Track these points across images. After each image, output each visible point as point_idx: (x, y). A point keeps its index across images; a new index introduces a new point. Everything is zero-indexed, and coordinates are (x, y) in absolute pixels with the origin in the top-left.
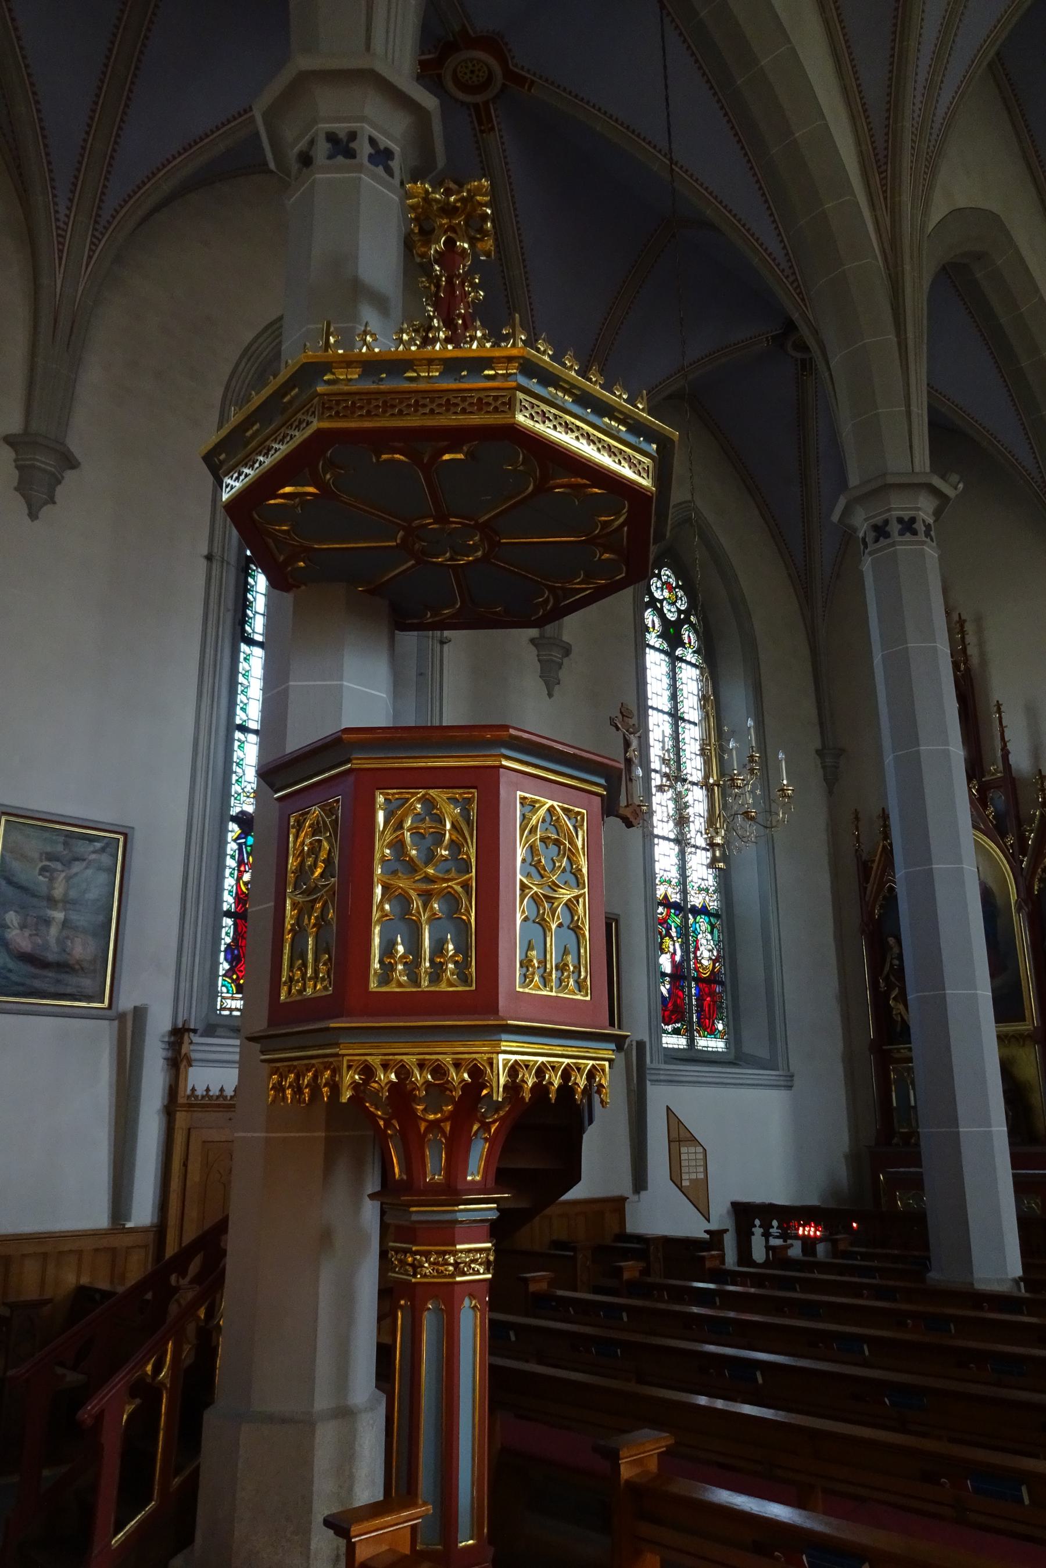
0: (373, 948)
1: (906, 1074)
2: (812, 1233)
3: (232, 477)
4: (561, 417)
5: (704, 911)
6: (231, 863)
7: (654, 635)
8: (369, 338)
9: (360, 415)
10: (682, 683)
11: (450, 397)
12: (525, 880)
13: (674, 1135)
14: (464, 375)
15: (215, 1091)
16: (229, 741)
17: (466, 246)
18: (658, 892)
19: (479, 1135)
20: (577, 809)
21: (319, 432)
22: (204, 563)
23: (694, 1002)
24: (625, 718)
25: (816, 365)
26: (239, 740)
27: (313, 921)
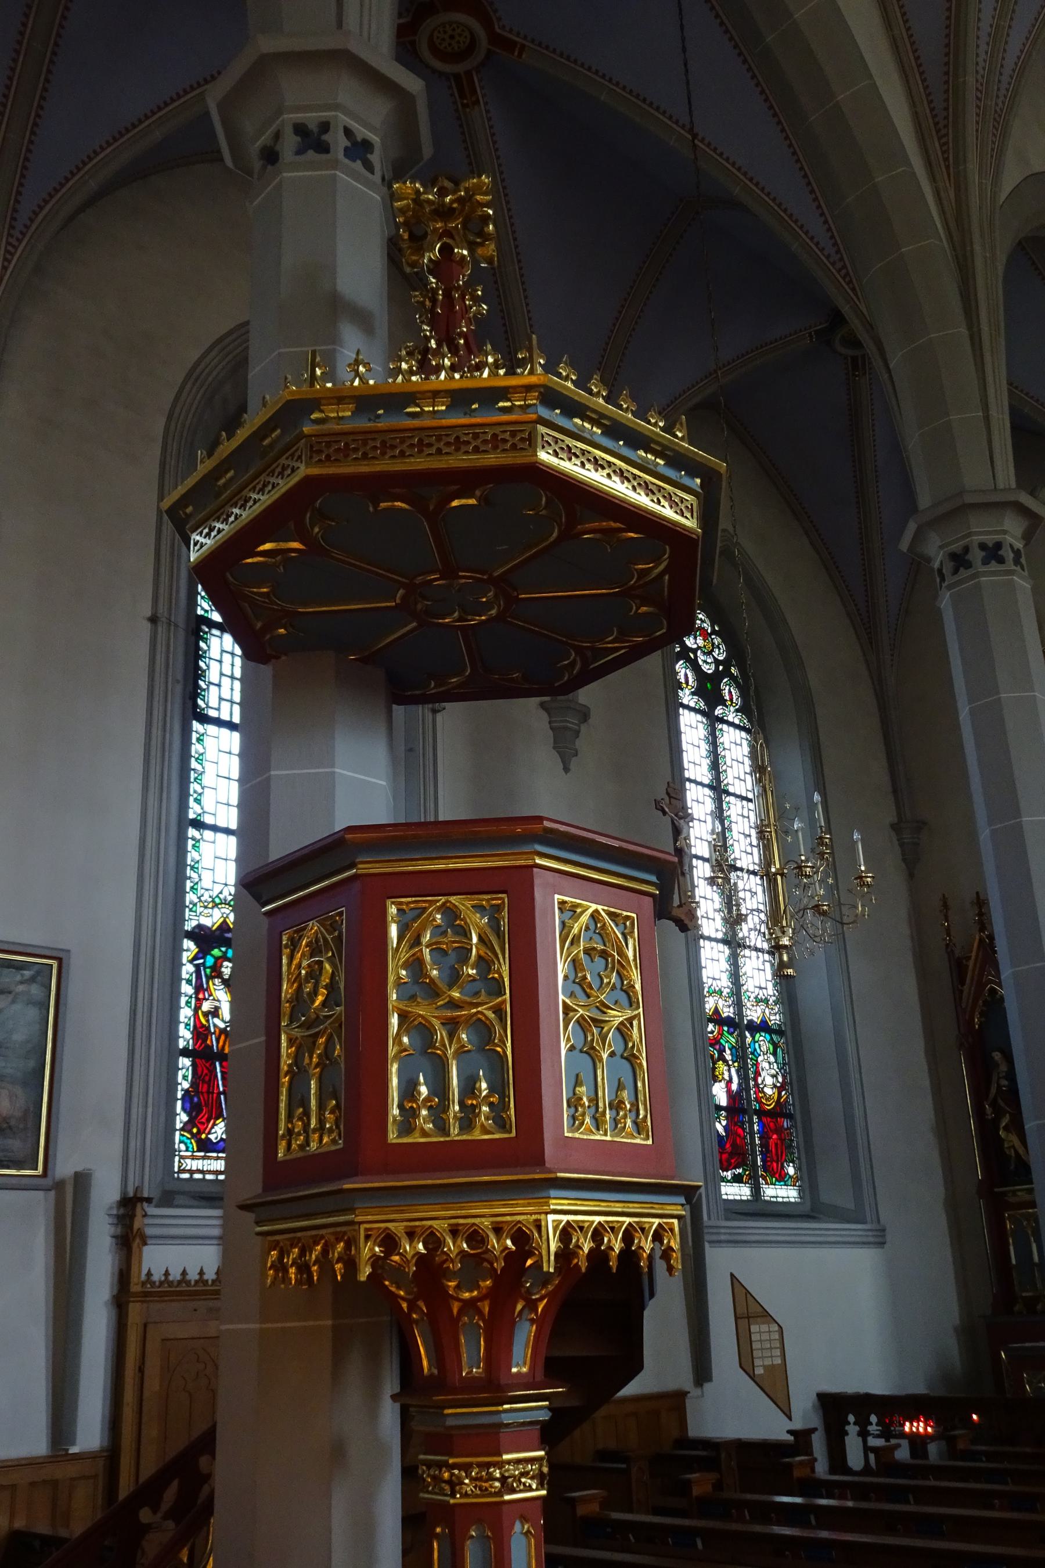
0: (390, 1091)
1: (1025, 1223)
2: (921, 1430)
3: (201, 533)
4: (589, 452)
5: (763, 1026)
6: (187, 989)
7: (687, 692)
8: (361, 369)
9: (356, 459)
10: (724, 749)
11: (460, 434)
12: (568, 1001)
13: (742, 1310)
14: (476, 409)
15: (175, 1275)
16: (182, 840)
17: (465, 252)
18: (707, 1006)
19: (524, 1316)
20: (625, 913)
21: (307, 480)
22: (148, 625)
23: (757, 1142)
24: (672, 800)
25: (870, 363)
26: (193, 839)
27: (315, 1060)
